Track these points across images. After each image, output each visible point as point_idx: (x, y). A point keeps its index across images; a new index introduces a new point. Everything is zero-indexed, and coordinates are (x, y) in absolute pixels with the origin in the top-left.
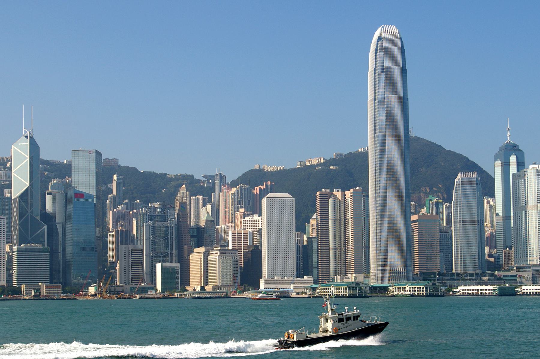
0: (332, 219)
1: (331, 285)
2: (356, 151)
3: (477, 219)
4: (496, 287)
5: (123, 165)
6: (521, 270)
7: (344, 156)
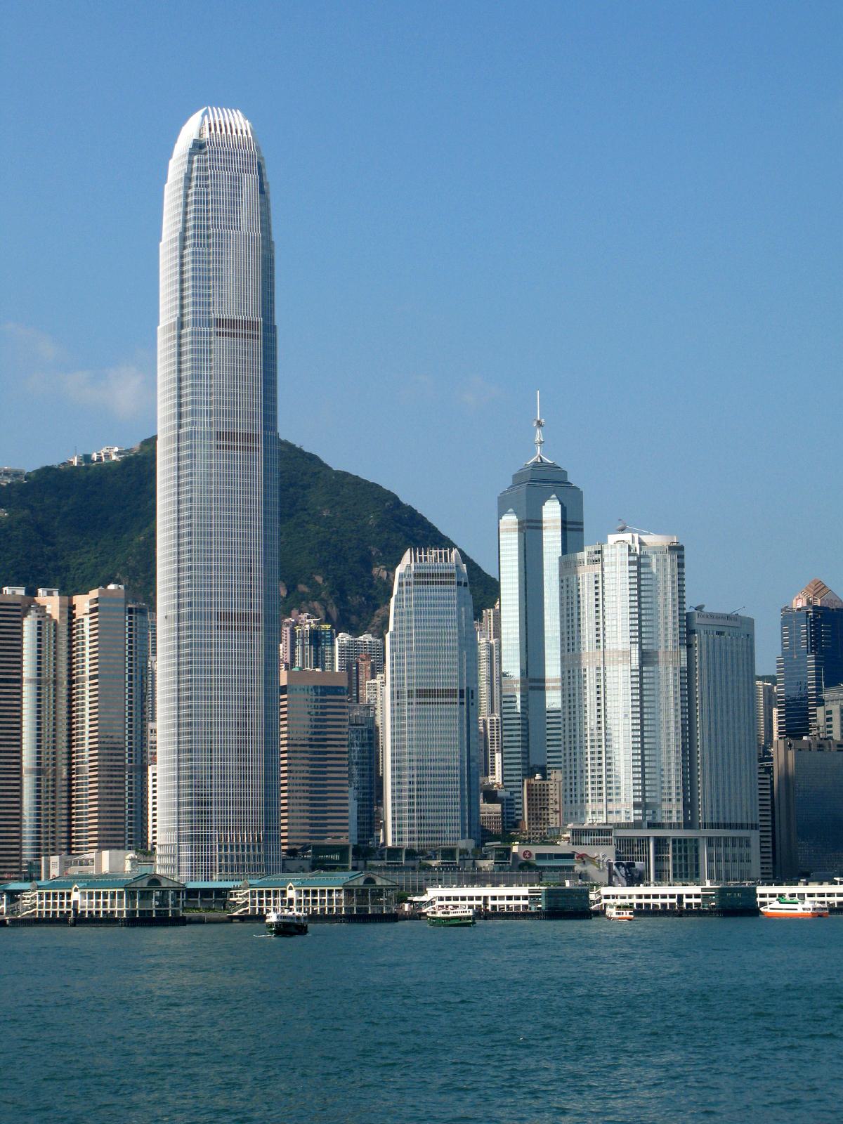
0: (30, 681)
1: (72, 884)
2: (63, 464)
3: (457, 687)
4: (537, 891)
6: (586, 839)
7: (26, 478)
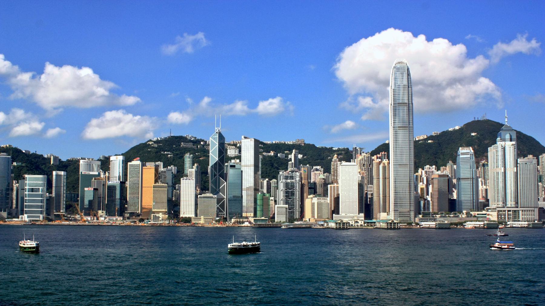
5: (308, 143)
6: (490, 210)
